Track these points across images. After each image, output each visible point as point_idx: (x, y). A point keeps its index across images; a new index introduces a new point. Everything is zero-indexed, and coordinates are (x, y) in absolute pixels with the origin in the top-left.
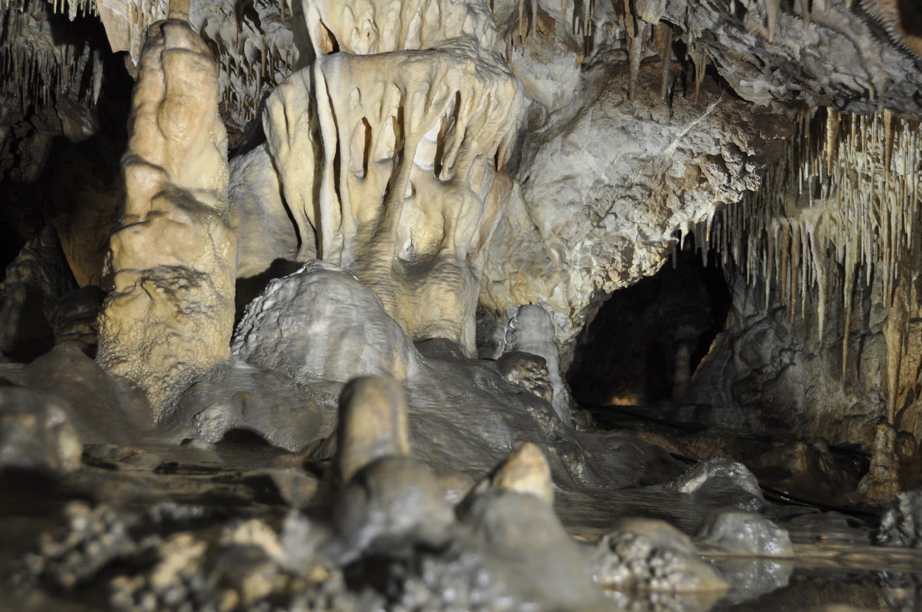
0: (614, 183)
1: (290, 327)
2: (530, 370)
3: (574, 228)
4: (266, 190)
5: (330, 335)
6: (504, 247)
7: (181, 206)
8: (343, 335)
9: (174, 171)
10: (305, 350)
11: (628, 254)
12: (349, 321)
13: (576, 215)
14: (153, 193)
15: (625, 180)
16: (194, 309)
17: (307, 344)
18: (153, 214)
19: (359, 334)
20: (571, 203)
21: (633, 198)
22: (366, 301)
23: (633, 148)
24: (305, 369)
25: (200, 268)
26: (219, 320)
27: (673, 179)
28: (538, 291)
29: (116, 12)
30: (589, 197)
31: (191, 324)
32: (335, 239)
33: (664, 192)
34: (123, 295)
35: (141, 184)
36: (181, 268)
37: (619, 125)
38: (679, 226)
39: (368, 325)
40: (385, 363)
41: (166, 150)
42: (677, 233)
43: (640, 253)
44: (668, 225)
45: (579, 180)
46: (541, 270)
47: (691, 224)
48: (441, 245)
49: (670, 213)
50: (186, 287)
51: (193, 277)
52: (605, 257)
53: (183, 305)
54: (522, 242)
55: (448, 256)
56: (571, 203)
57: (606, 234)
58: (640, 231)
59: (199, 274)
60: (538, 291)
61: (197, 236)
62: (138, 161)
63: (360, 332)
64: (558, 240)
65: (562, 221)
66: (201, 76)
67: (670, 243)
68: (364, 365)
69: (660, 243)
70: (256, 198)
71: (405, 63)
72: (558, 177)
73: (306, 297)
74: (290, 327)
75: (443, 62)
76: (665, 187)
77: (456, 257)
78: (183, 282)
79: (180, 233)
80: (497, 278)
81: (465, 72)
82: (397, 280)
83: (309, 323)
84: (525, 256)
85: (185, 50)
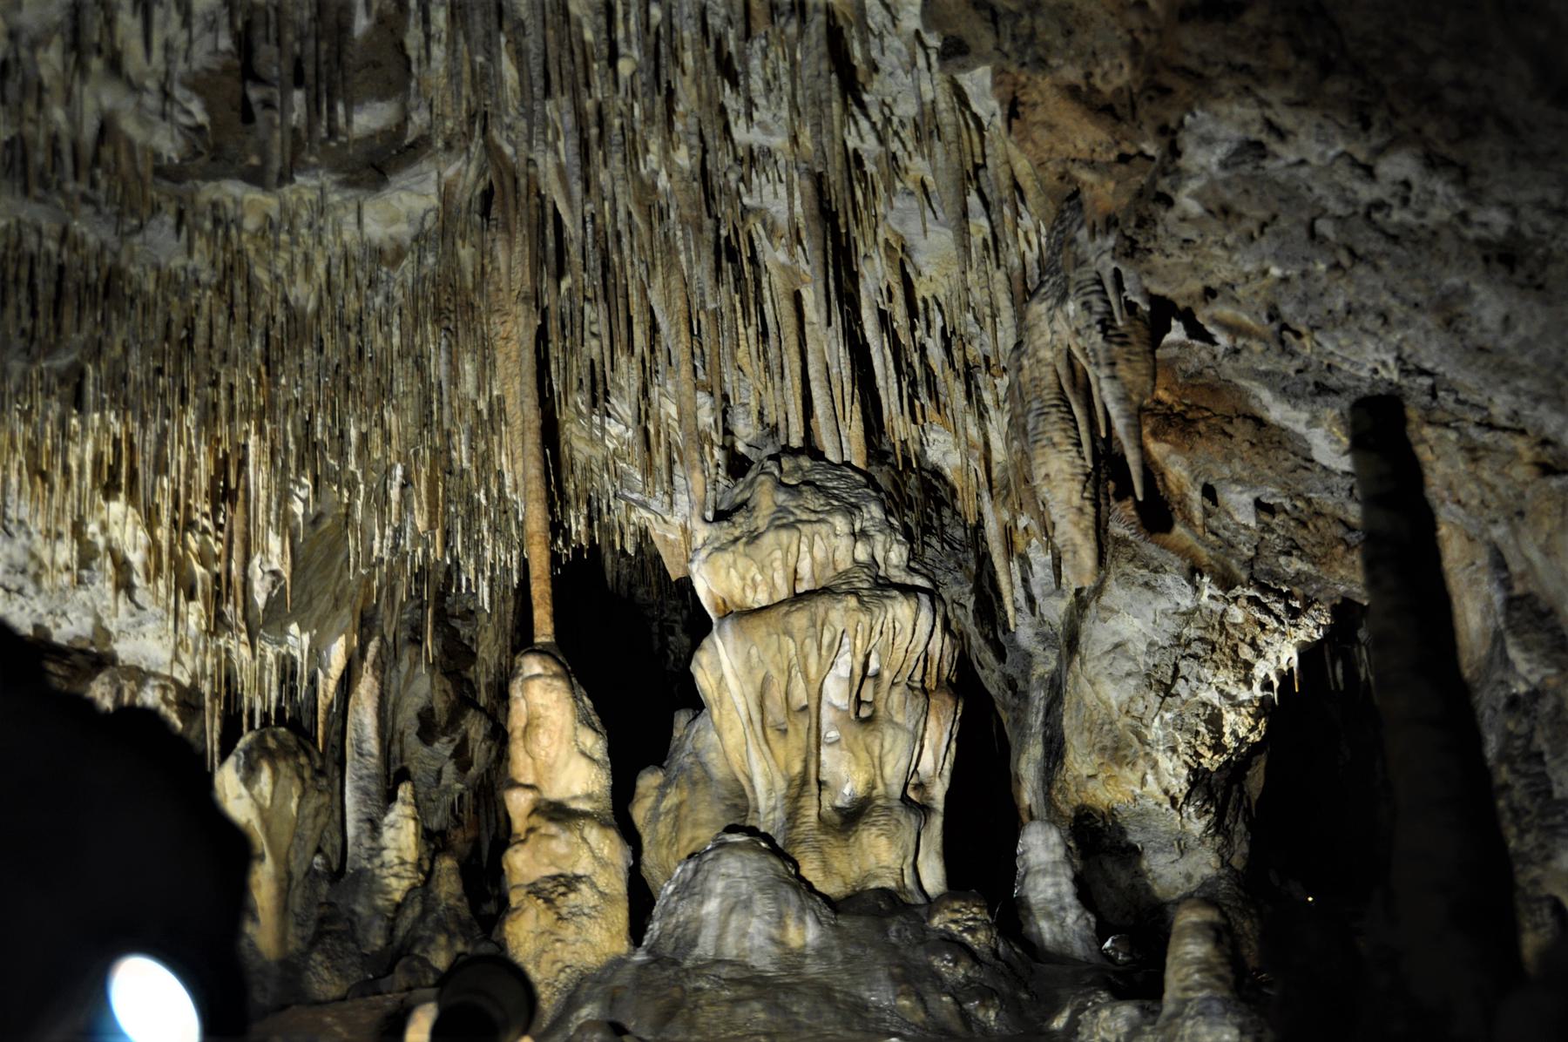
0: (1167, 644)
1: (684, 911)
2: (958, 911)
3: (1140, 705)
4: (713, 755)
5: (721, 912)
6: (1086, 734)
7: (551, 819)
8: (732, 910)
9: (545, 787)
10: (698, 931)
11: (1215, 721)
12: (738, 895)
13: (1137, 688)
14: (528, 811)
15: (1178, 637)
16: (577, 912)
17: (700, 923)
18: (531, 830)
19: (746, 907)
20: (1129, 675)
21: (1195, 657)
22: (759, 870)
23: (1163, 604)
24: (697, 951)
25: (580, 872)
26: (605, 918)
27: (1234, 625)
28: (1130, 783)
29: (671, 536)
30: (1146, 664)
31: (572, 928)
32: (769, 799)
33: (1230, 643)
34: (516, 909)
35: (518, 803)
36: (561, 876)
37: (1141, 581)
38: (1267, 676)
39: (758, 896)
40: (775, 932)
41: (535, 769)
42: (1267, 685)
43: (1229, 717)
44: (1253, 677)
45: (1130, 645)
46: (1125, 756)
47: (1280, 673)
48: (872, 786)
49: (1249, 666)
50: (564, 894)
51: (570, 882)
52: (1188, 730)
53: (564, 911)
54: (1103, 724)
55: (878, 797)
56: (1129, 675)
57: (1184, 702)
58: (1221, 692)
59: (578, 878)
60: (1130, 783)
61: (569, 844)
62: (514, 784)
63: (747, 905)
64: (1128, 720)
65: (1124, 697)
66: (554, 696)
67: (1262, 699)
68: (752, 938)
69: (1250, 701)
70: (703, 765)
71: (787, 613)
72: (1107, 647)
73: (700, 877)
74: (684, 911)
75: (821, 605)
76: (1228, 636)
77: (886, 797)
78: (562, 889)
79: (554, 844)
80: (1091, 772)
81: (846, 610)
82: (827, 833)
83: (701, 903)
84: (1108, 742)
85: (539, 676)
